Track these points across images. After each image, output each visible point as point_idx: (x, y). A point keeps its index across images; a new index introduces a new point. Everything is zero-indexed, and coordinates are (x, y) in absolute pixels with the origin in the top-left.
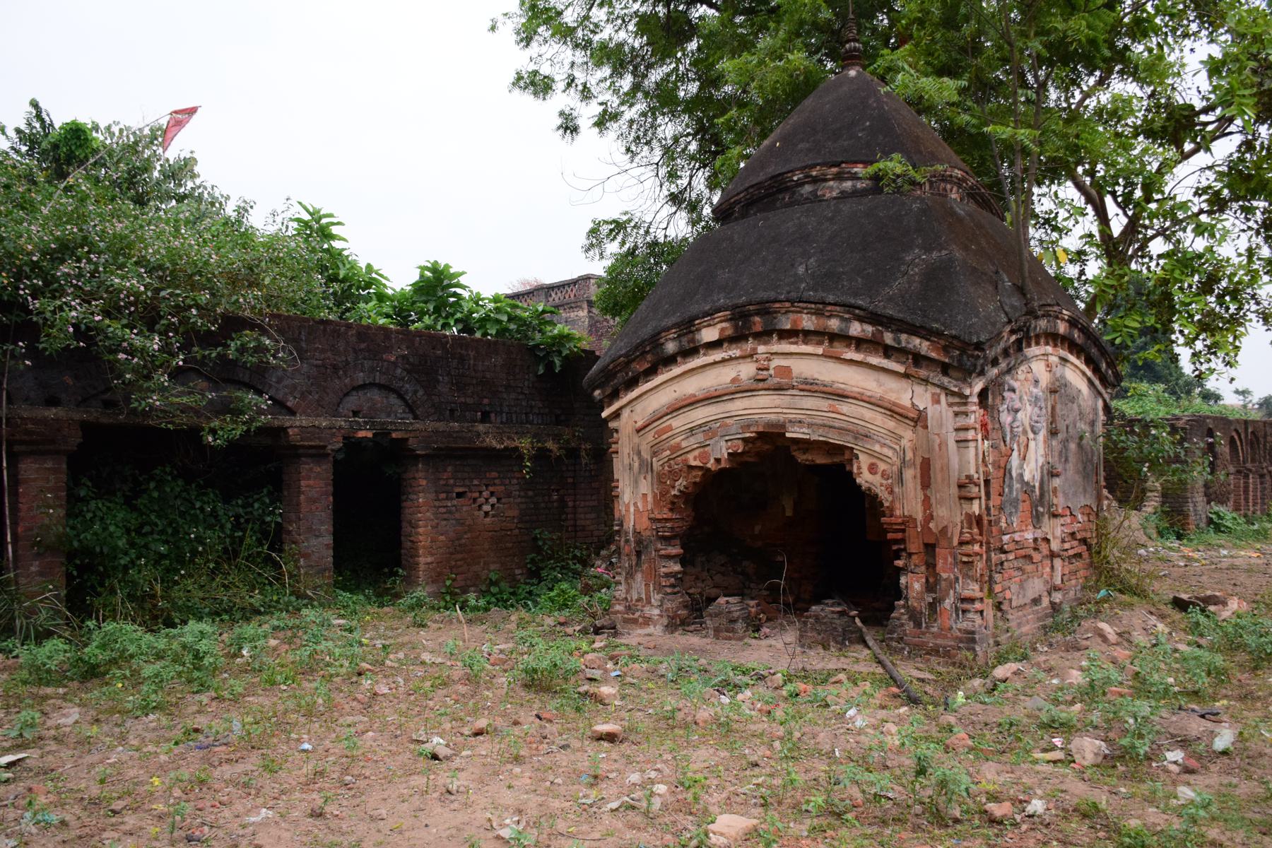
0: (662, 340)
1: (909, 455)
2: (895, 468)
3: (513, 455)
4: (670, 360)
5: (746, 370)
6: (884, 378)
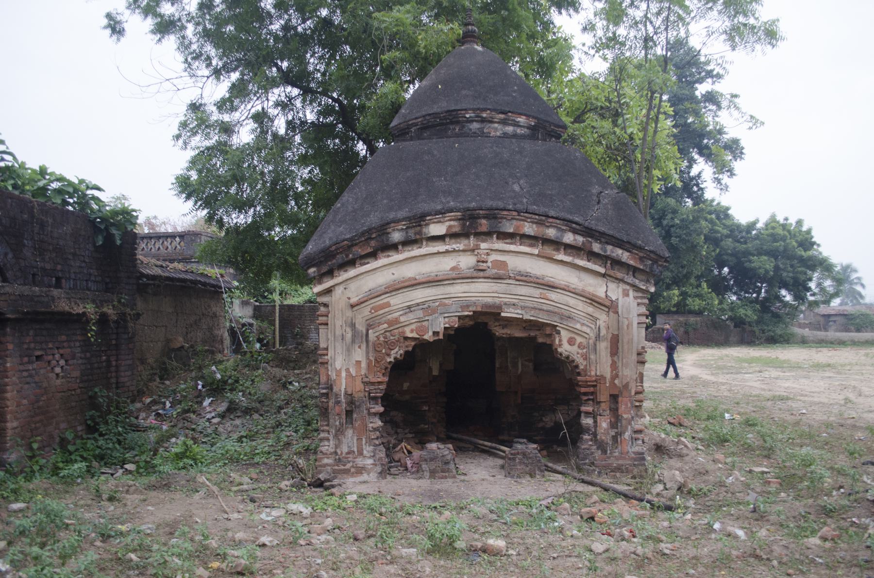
0: (390, 230)
1: (603, 332)
2: (591, 342)
3: (81, 320)
4: (394, 247)
5: (467, 262)
6: (585, 276)
